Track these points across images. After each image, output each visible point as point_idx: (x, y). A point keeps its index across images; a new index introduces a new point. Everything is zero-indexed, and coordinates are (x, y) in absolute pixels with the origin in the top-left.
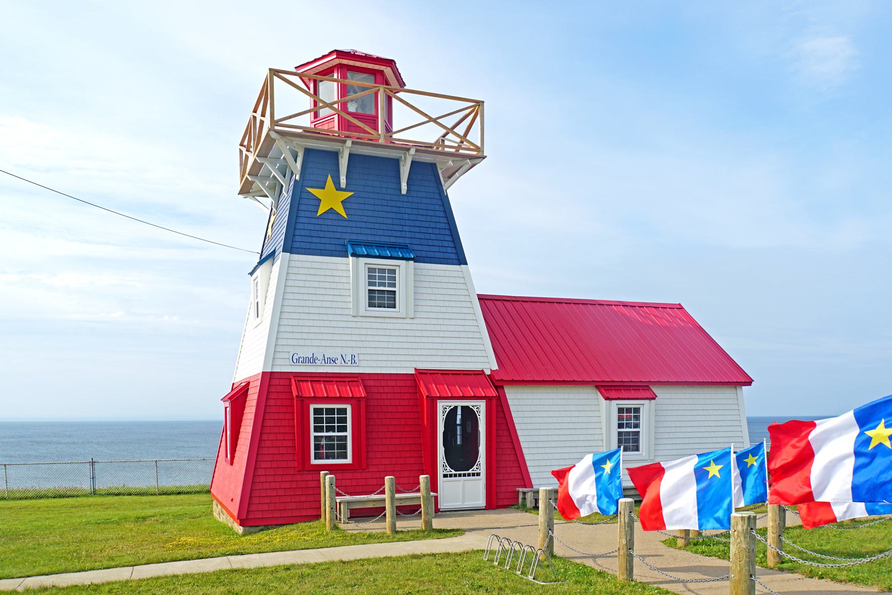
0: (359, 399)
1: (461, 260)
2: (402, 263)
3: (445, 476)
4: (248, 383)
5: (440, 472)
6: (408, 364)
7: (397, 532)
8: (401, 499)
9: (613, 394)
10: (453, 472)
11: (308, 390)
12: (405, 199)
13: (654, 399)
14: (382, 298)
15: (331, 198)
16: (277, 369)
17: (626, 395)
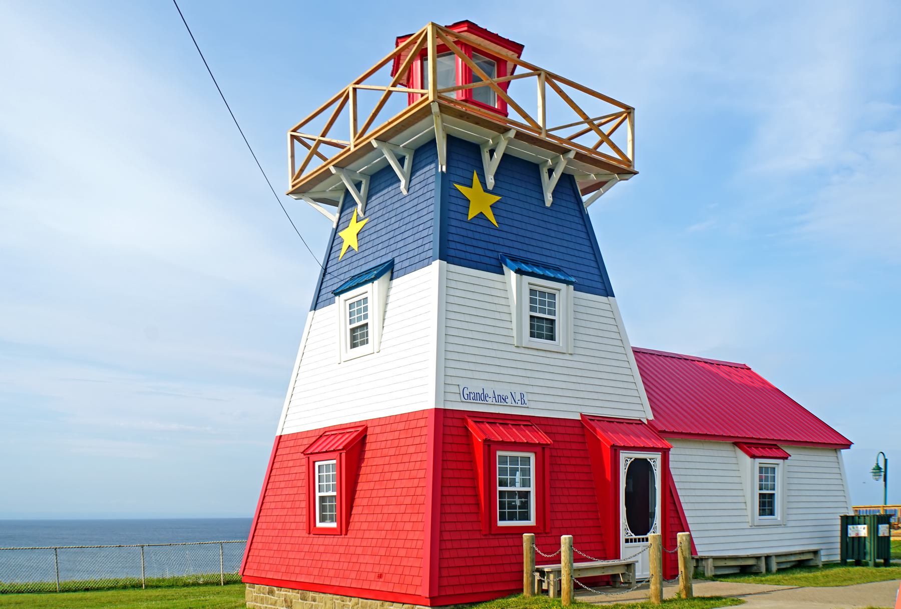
0: (543, 447)
1: (608, 292)
2: (562, 286)
3: (627, 541)
4: (366, 429)
5: (623, 537)
6: (573, 408)
7: (665, 601)
8: (579, 570)
9: (755, 451)
10: (634, 536)
11: (497, 433)
12: (549, 213)
13: (787, 458)
14: (542, 328)
15: (480, 201)
16: (449, 406)
17: (765, 454)
